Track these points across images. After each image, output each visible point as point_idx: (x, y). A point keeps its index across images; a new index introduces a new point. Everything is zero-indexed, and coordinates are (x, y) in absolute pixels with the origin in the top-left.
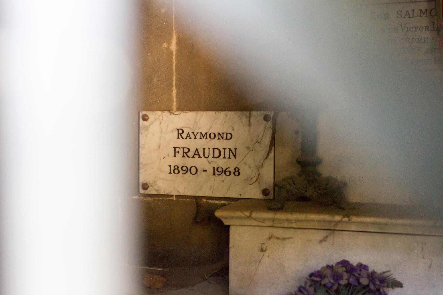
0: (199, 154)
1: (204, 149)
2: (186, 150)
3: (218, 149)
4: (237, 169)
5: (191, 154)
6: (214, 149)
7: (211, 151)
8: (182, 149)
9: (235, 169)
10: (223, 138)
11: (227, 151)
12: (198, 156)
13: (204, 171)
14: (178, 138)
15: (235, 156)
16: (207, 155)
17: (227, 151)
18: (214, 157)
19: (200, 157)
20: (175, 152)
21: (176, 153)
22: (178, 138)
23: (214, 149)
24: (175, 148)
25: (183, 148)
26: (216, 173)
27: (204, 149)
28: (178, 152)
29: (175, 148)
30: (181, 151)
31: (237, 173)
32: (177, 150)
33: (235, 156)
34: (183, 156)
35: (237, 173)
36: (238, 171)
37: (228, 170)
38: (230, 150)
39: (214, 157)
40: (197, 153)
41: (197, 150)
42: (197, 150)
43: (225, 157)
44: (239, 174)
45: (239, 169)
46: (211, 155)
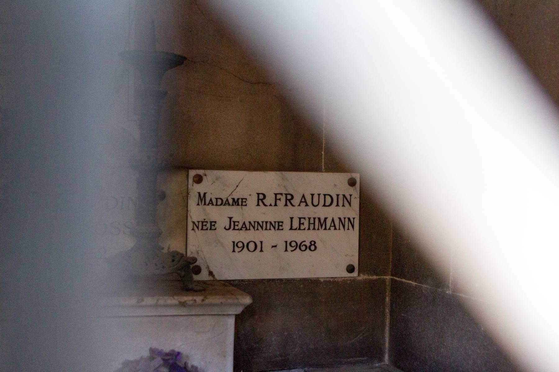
0: (305, 202)
1: (312, 195)
2: (289, 197)
3: (249, 251)
4: (313, 243)
5: (296, 201)
6: (325, 195)
7: (322, 197)
8: (284, 196)
9: (311, 242)
10: (274, 228)
11: (341, 197)
12: (304, 204)
13: (273, 247)
14: (258, 205)
15: (350, 204)
16: (316, 203)
17: (341, 197)
18: (324, 205)
19: (307, 205)
20: (276, 199)
21: (278, 201)
22: (258, 205)
23: (325, 195)
24: (276, 194)
25: (286, 194)
26: (289, 248)
27: (312, 195)
28: (280, 199)
29: (276, 194)
30: (283, 198)
31: (313, 248)
32: (279, 196)
33: (350, 204)
34: (286, 205)
35: (313, 248)
36: (314, 245)
37: (304, 243)
38: (344, 196)
39: (324, 205)
40: (303, 200)
41: (303, 196)
42: (303, 196)
43: (338, 205)
44: (316, 248)
45: (315, 242)
46: (322, 203)
